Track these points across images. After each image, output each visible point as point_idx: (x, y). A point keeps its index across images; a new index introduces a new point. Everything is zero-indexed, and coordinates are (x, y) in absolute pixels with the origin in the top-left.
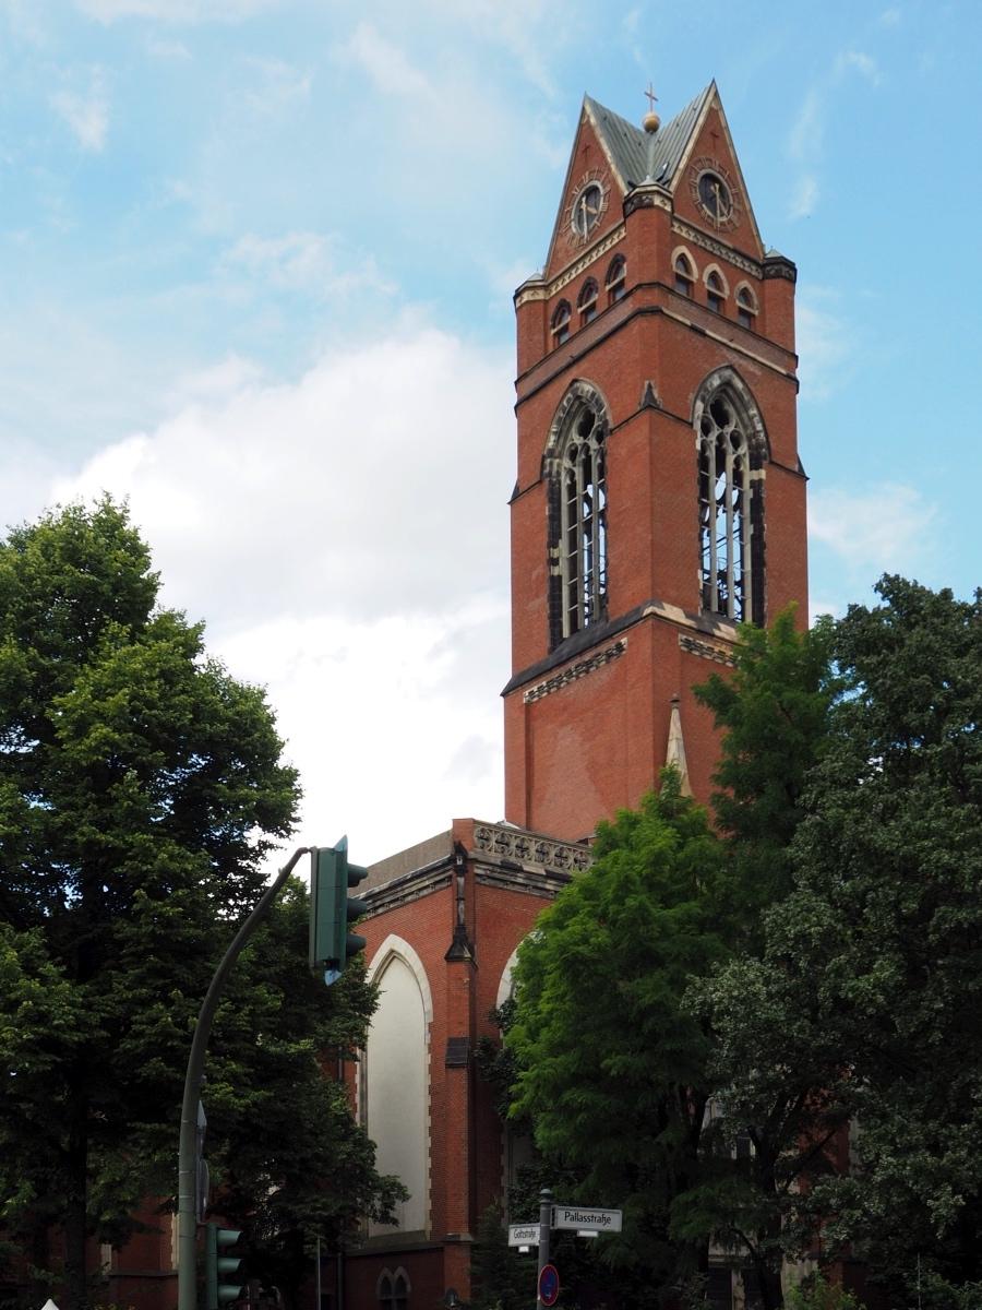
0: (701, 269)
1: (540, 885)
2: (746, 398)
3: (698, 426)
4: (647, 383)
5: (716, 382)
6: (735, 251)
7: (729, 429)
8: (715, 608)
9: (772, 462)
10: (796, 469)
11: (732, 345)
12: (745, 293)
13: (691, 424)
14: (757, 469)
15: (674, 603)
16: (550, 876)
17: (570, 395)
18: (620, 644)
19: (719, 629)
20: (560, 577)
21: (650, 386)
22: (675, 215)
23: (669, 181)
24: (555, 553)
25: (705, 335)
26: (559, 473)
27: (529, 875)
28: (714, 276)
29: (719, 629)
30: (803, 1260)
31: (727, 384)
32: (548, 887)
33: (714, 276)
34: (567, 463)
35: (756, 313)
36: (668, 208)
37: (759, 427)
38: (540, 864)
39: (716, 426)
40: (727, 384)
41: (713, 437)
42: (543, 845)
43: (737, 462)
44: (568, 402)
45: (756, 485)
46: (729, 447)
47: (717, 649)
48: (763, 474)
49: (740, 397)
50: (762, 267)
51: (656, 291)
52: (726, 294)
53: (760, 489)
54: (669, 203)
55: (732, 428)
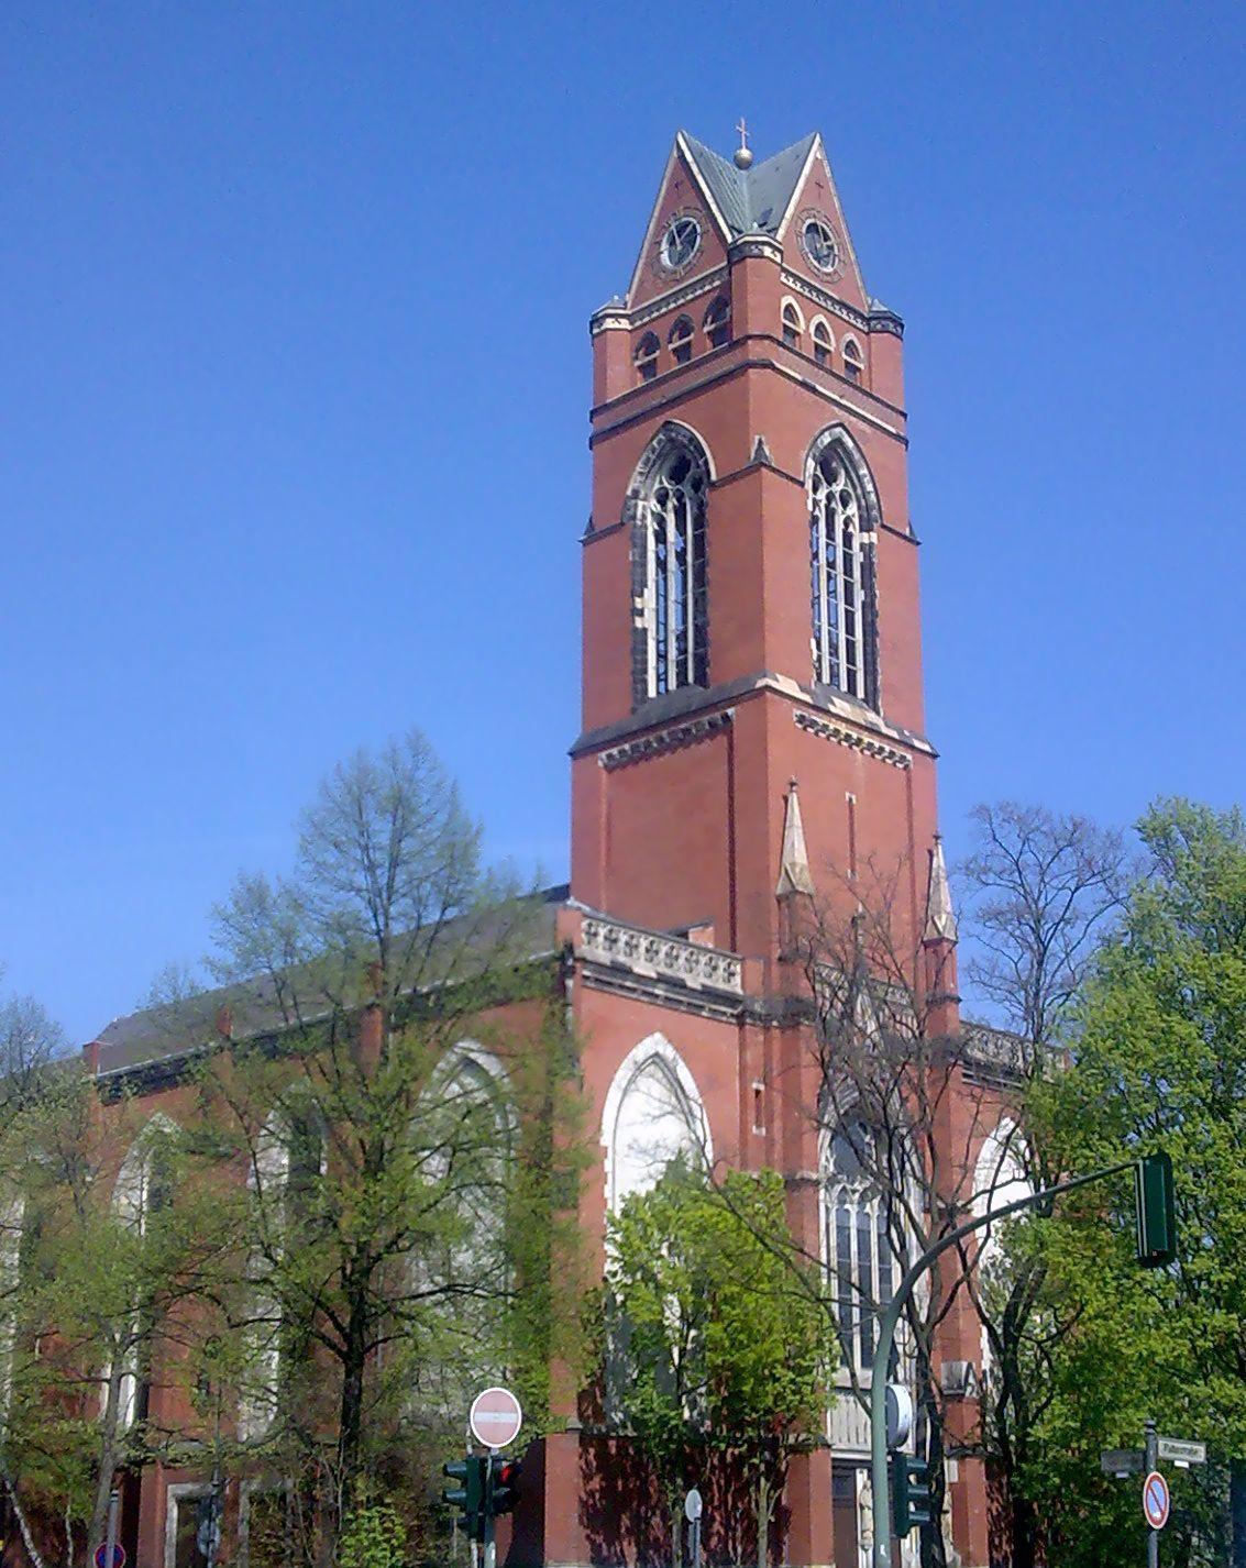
0: (808, 321)
1: (650, 990)
2: (857, 456)
3: (809, 485)
4: (757, 437)
5: (826, 439)
6: (839, 303)
7: (837, 488)
8: (826, 679)
9: (883, 526)
10: (907, 533)
11: (843, 402)
12: (850, 346)
13: (802, 484)
14: (868, 531)
15: (788, 675)
16: (661, 979)
17: (661, 436)
18: (726, 715)
19: (833, 704)
20: (645, 630)
21: (760, 442)
22: (784, 265)
23: (776, 229)
24: (638, 603)
25: (814, 390)
26: (644, 517)
27: (640, 978)
28: (820, 328)
29: (833, 704)
30: (595, 1289)
31: (838, 441)
32: (657, 992)
33: (850, 346)
34: (654, 505)
35: (862, 366)
36: (778, 259)
37: (870, 487)
38: (650, 965)
39: (825, 484)
40: (838, 441)
41: (822, 495)
42: (611, 931)
43: (847, 522)
44: (659, 443)
45: (867, 549)
46: (837, 505)
47: (832, 727)
48: (874, 537)
49: (849, 455)
50: (867, 320)
51: (767, 342)
52: (801, 328)
53: (870, 552)
54: (779, 255)
55: (841, 487)
